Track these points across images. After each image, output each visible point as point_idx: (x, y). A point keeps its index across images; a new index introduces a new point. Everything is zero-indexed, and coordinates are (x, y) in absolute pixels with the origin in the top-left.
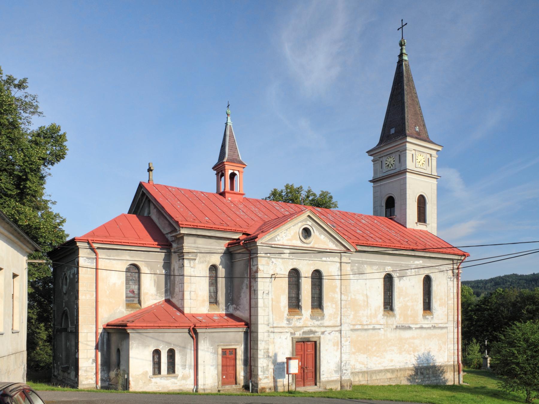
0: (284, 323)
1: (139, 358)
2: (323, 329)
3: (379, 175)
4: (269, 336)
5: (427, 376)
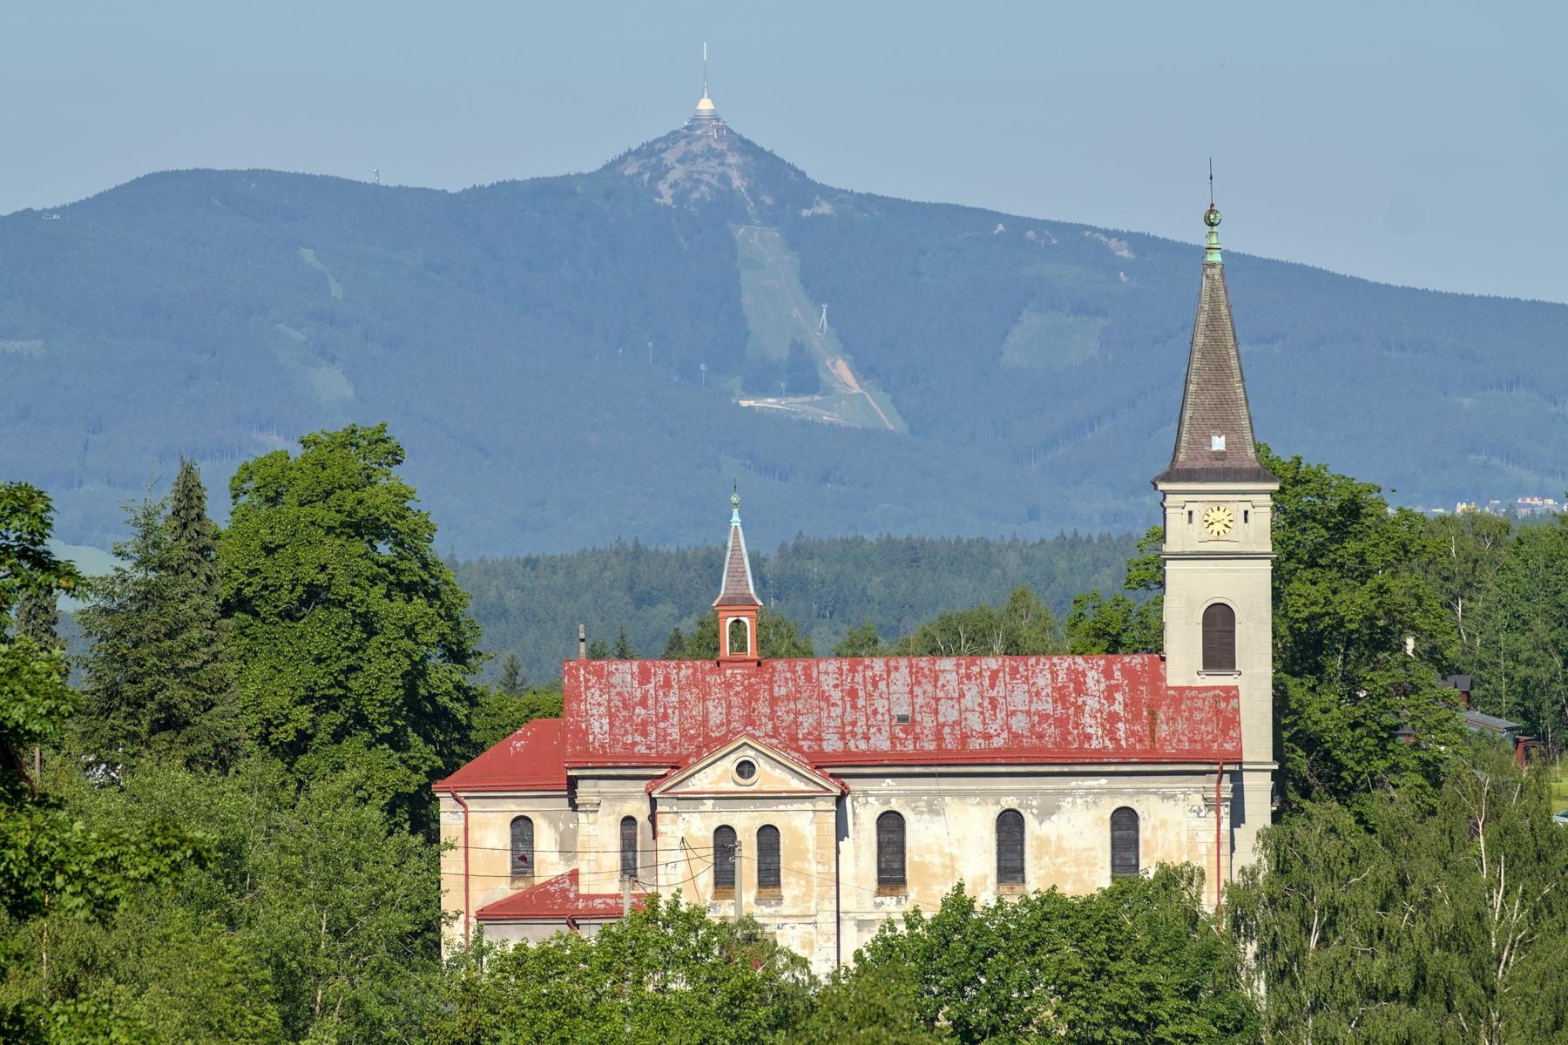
2: (780, 921)
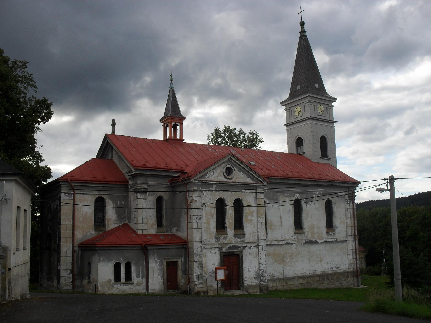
0: (213, 240)
1: (104, 271)
2: (244, 245)
3: (292, 120)
4: (202, 251)
5: (332, 281)
